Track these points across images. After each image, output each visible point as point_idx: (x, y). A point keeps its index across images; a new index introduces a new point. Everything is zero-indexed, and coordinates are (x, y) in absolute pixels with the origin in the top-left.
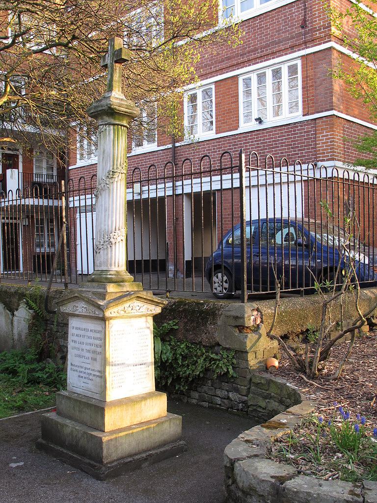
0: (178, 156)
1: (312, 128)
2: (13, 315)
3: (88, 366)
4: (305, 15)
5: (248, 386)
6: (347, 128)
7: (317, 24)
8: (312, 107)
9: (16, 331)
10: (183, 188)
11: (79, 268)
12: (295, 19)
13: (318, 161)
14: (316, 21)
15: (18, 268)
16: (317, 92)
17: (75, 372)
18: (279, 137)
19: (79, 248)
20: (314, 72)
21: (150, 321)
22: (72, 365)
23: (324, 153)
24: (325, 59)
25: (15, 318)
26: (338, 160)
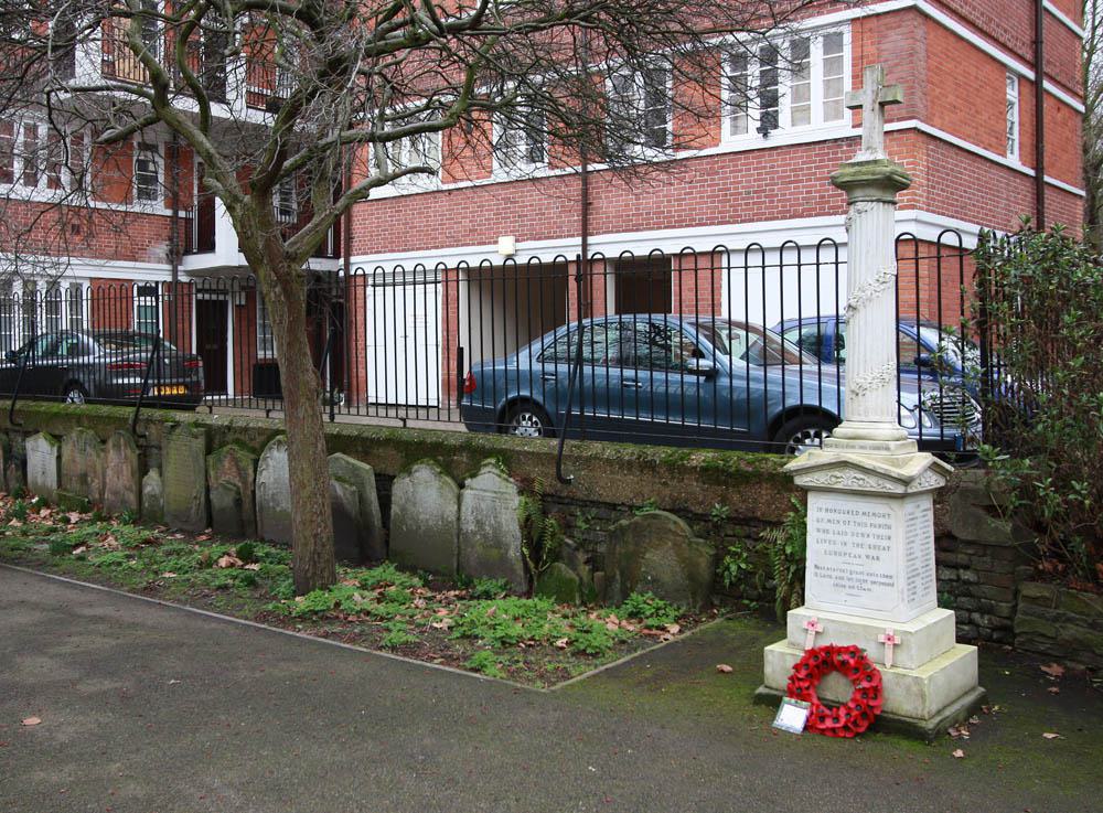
0: (593, 188)
3: (860, 569)
5: (1014, 603)
6: (932, 150)
10: (917, 254)
11: (371, 392)
15: (224, 390)
18: (803, 163)
20: (878, 49)
21: (927, 504)
22: (816, 566)
24: (899, 27)
25: (467, 493)
26: (921, 209)
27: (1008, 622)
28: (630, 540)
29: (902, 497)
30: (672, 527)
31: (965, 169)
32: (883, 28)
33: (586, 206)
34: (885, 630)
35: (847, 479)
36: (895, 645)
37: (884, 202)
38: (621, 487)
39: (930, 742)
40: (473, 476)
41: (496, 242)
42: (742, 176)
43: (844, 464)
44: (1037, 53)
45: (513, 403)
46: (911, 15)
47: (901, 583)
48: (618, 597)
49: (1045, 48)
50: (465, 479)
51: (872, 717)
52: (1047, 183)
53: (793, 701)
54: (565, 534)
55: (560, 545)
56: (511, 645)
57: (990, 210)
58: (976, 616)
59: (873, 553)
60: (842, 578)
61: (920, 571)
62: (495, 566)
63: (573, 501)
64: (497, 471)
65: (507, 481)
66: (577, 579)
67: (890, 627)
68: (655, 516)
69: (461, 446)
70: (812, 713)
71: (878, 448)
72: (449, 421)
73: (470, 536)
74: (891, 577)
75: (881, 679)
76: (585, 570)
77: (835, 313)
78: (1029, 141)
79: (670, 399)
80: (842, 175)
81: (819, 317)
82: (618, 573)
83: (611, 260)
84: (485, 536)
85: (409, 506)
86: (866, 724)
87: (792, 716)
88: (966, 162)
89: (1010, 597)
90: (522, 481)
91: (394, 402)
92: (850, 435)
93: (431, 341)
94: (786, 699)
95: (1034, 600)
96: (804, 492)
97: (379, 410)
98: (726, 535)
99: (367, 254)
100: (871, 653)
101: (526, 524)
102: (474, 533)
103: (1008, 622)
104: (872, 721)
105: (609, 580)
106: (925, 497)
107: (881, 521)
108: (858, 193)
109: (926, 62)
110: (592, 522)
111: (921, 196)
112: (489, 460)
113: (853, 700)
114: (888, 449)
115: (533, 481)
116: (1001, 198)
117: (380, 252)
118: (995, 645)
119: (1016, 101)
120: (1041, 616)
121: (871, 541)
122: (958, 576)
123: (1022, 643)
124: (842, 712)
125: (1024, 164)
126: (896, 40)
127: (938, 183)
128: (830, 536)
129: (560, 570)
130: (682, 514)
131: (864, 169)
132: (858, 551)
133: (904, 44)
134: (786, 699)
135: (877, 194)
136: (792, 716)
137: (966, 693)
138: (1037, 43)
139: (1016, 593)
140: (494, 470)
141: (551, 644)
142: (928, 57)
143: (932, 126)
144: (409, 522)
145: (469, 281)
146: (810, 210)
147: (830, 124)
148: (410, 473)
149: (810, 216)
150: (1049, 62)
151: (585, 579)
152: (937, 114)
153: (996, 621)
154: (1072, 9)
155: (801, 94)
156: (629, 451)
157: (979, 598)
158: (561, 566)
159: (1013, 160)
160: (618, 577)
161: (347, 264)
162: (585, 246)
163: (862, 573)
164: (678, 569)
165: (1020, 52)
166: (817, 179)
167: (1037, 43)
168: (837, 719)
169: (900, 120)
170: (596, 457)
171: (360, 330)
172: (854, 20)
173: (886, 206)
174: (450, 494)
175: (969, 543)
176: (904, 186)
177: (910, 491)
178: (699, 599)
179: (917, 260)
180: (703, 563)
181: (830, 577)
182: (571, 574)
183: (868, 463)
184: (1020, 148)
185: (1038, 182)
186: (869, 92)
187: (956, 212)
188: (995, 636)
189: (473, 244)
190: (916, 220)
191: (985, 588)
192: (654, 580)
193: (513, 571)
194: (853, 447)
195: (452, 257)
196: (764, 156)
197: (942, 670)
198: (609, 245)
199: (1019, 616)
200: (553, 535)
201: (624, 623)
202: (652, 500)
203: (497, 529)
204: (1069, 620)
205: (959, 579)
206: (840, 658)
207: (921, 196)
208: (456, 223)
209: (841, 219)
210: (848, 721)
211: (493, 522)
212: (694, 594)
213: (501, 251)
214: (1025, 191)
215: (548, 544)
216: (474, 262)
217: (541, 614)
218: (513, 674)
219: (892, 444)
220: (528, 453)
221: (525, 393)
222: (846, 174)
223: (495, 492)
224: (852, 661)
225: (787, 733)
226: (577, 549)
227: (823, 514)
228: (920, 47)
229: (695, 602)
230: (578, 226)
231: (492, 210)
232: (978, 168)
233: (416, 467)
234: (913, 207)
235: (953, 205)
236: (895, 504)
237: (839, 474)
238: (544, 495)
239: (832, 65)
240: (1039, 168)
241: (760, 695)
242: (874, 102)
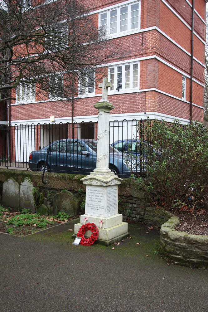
1: (144, 95)
2: (20, 185)
3: (96, 204)
4: (143, 40)
7: (148, 46)
8: (144, 85)
9: (21, 192)
11: (17, 159)
12: (137, 42)
13: (146, 111)
14: (148, 44)
16: (147, 79)
17: (90, 207)
18: (128, 98)
19: (16, 147)
21: (116, 188)
22: (88, 204)
23: (149, 108)
24: (151, 63)
25: (21, 186)
26: (155, 112)
27: (143, 217)
28: (59, 198)
29: (106, 186)
30: (69, 195)
31: (169, 101)
32: (147, 63)
33: (73, 108)
34: (101, 219)
35: (94, 182)
36: (102, 223)
37: (106, 112)
38: (57, 184)
39: (108, 246)
40: (23, 182)
41: (49, 118)
42: (140, 102)
43: (93, 179)
44: (191, 71)
45: (40, 163)
46: (154, 60)
47: (105, 207)
48: (56, 212)
49: (193, 70)
50: (21, 183)
51: (95, 240)
52: (193, 105)
53: (78, 237)
54: (45, 197)
55: (43, 200)
56: (21, 226)
57: (177, 112)
58: (136, 215)
59: (99, 200)
60: (93, 207)
61: (112, 205)
62: (27, 206)
63: (47, 188)
64: (28, 181)
65: (31, 183)
66: (47, 208)
67: (102, 219)
68: (65, 192)
69: (20, 174)
70: (81, 240)
71: (102, 175)
72: (21, 167)
73: (22, 198)
74: (103, 206)
75: (98, 231)
76: (49, 206)
77: (126, 139)
78: (189, 94)
79: (78, 161)
80: (96, 105)
81: (123, 140)
82: (56, 206)
83: (79, 123)
84: (25, 198)
85: (7, 190)
86: (93, 242)
87: (77, 241)
88: (170, 99)
89: (144, 211)
90: (34, 183)
91: (23, 161)
92: (96, 171)
93: (33, 144)
94: (77, 237)
95: (148, 211)
96: (85, 185)
97: (24, 164)
98: (82, 197)
99: (15, 120)
100: (97, 224)
101: (35, 194)
102: (23, 197)
103: (143, 217)
104: (96, 241)
105: (54, 208)
106: (115, 186)
107: (101, 193)
108: (100, 110)
109: (158, 73)
110: (52, 194)
111: (156, 108)
112: (26, 178)
113: (91, 236)
114: (104, 175)
115: (37, 183)
116: (180, 109)
117: (19, 120)
118: (140, 222)
119: (185, 84)
120: (150, 215)
121: (99, 197)
122: (133, 206)
123: (146, 222)
124: (88, 240)
125: (187, 100)
126: (151, 67)
127: (161, 105)
128: (91, 197)
129: (43, 206)
130: (72, 191)
131: (101, 104)
132: (97, 200)
133: (152, 68)
134: (77, 237)
135: (104, 110)
136: (77, 241)
137: (122, 234)
138: (191, 69)
139: (145, 210)
140: (28, 180)
141: (32, 225)
142: (159, 72)
143: (160, 90)
144: (7, 194)
145: (44, 129)
146: (129, 111)
147: (134, 88)
148: (7, 181)
149: (129, 113)
150: (195, 74)
151: (49, 208)
152: (161, 87)
153: (141, 217)
154: (202, 60)
155: (127, 80)
156: (61, 175)
157: (137, 211)
158: (43, 205)
159: (184, 99)
160: (56, 208)
161: (10, 123)
162: (72, 119)
163: (97, 206)
164: (70, 205)
165: (186, 71)
166: (131, 103)
167: (191, 69)
168: (87, 241)
169: (151, 88)
170: (52, 177)
171: (14, 141)
172: (140, 61)
173: (107, 113)
174: (17, 187)
175: (136, 198)
176: (112, 109)
177: (107, 185)
178: (75, 213)
179: (37, 129)
180: (76, 204)
181: (90, 206)
182: (46, 207)
183: (98, 178)
184: (186, 96)
185: (191, 105)
186: (104, 84)
187: (167, 112)
188: (140, 220)
189: (44, 118)
190: (154, 115)
191: (139, 209)
192: (65, 208)
193: (32, 207)
194: (97, 174)
195: (36, 122)
196: (118, 96)
197: (114, 229)
198: (79, 119)
199: (145, 215)
200: (41, 197)
201: (55, 219)
202: (65, 188)
203: (28, 196)
204: (155, 216)
205: (133, 207)
206: (89, 226)
207: (156, 108)
208: (39, 112)
209: (97, 116)
210: (89, 241)
211: (27, 194)
212: (74, 212)
213: (51, 120)
214: (187, 107)
215: (40, 199)
216: (42, 123)
217: (32, 217)
218: (16, 234)
219: (105, 174)
220: (36, 176)
221: (43, 159)
222: (97, 105)
223: (28, 186)
224: (92, 227)
225: (75, 245)
226: (48, 201)
227: (89, 191)
228: (157, 69)
229: (74, 214)
230: (71, 114)
231: (49, 109)
232: (173, 101)
233: (9, 180)
234: (154, 111)
235: (165, 111)
236: (104, 188)
237: (92, 181)
238: (40, 187)
239: (135, 72)
240: (191, 101)
241: (73, 236)
242: (105, 86)
